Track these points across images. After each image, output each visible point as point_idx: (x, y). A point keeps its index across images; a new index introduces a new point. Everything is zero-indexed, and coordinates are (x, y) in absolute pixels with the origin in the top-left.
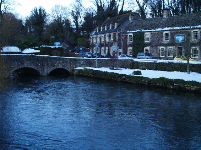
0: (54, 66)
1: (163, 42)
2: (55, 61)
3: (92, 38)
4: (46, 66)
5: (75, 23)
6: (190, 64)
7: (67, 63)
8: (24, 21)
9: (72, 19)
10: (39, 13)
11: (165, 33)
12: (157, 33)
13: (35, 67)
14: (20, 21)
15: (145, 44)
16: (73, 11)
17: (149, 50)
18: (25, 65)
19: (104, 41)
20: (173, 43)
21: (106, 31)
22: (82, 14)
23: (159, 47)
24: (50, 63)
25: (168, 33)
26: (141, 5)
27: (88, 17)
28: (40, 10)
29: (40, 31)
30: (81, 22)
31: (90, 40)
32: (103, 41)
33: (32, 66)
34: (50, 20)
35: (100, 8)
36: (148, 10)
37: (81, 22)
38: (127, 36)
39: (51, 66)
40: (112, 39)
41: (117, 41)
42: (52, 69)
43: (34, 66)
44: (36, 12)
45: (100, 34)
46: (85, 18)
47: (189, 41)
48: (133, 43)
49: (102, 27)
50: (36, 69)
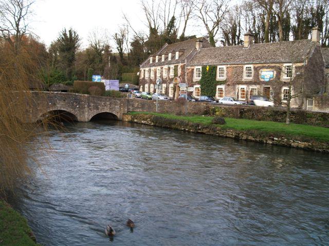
0: (97, 109)
3: (142, 71)
4: (86, 109)
5: (118, 50)
7: (116, 105)
8: (48, 46)
10: (68, 35)
11: (284, 90)
12: (236, 67)
14: (42, 47)
15: (218, 82)
16: (116, 34)
17: (223, 89)
18: (58, 107)
19: (160, 77)
20: (257, 82)
21: (164, 62)
23: (237, 86)
25: (250, 67)
27: (136, 44)
28: (70, 31)
29: (71, 60)
30: (127, 49)
31: (140, 75)
32: (159, 75)
34: (84, 45)
35: (153, 31)
36: (219, 37)
37: (127, 49)
38: (193, 69)
40: (172, 74)
41: (179, 77)
42: (95, 112)
44: (65, 35)
45: (155, 66)
46: (132, 44)
47: (279, 79)
48: (201, 79)
49: (157, 57)
50: (72, 112)
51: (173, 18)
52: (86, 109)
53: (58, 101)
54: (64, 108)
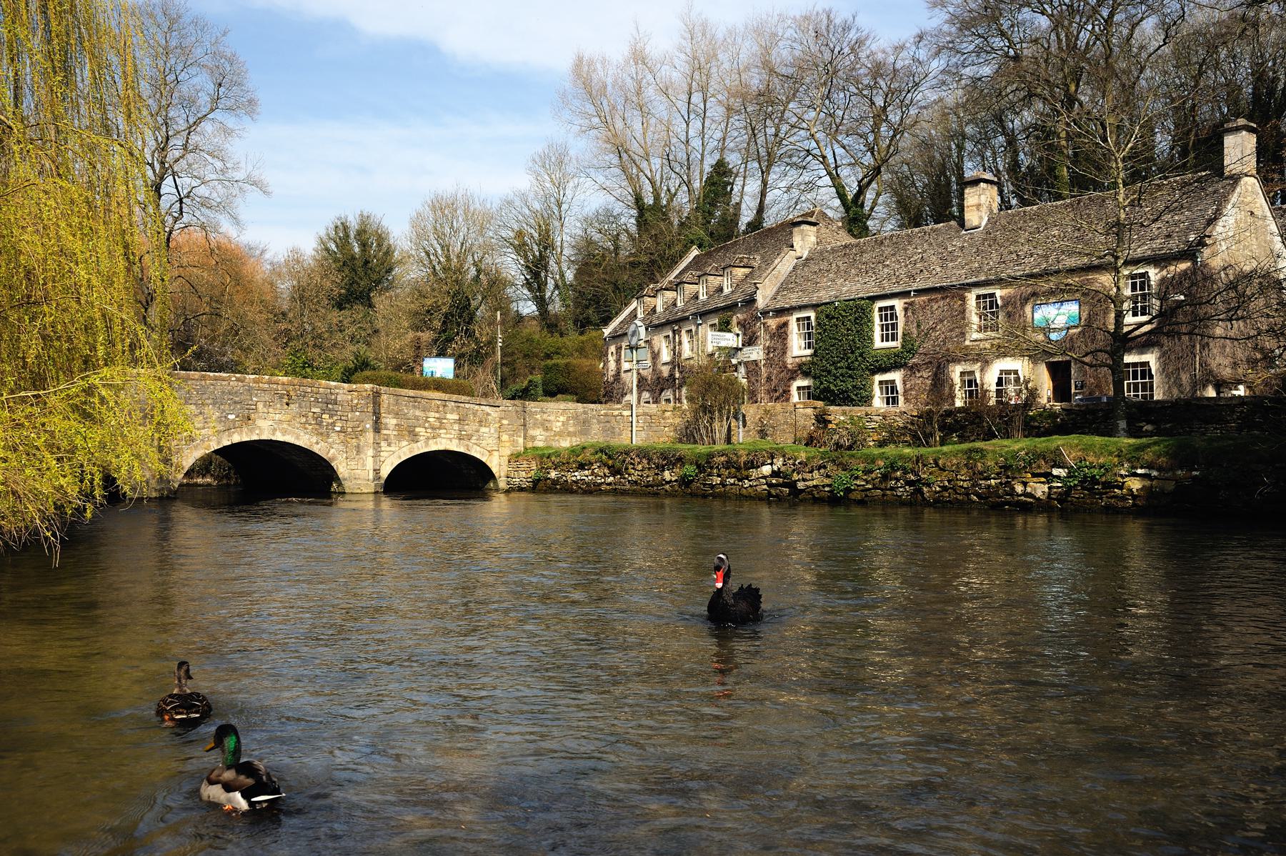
0: (414, 437)
1: (967, 343)
2: (418, 413)
6: (1221, 143)
9: (511, 267)
13: (314, 440)
22: (565, 244)
24: (394, 421)
26: (852, 188)
27: (589, 260)
33: (298, 438)
39: (400, 437)
43: (307, 436)
50: (316, 449)
51: (721, 169)
52: (370, 436)
53: (260, 406)
54: (284, 432)
